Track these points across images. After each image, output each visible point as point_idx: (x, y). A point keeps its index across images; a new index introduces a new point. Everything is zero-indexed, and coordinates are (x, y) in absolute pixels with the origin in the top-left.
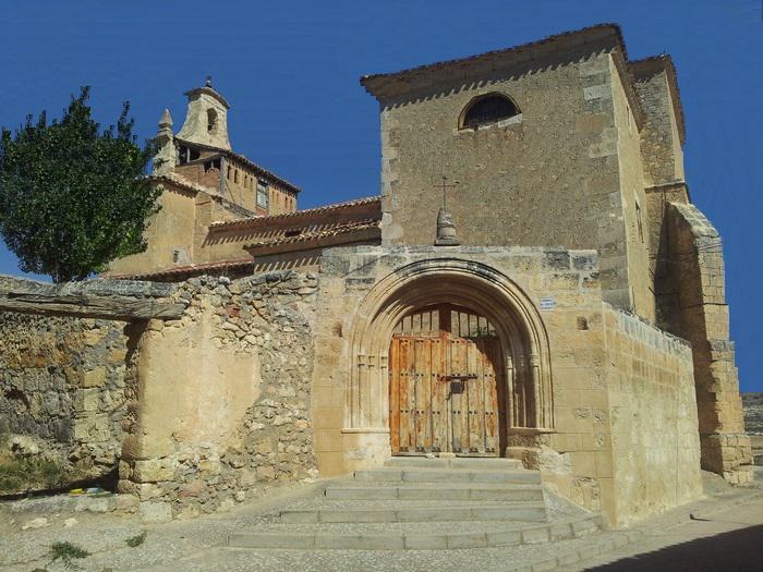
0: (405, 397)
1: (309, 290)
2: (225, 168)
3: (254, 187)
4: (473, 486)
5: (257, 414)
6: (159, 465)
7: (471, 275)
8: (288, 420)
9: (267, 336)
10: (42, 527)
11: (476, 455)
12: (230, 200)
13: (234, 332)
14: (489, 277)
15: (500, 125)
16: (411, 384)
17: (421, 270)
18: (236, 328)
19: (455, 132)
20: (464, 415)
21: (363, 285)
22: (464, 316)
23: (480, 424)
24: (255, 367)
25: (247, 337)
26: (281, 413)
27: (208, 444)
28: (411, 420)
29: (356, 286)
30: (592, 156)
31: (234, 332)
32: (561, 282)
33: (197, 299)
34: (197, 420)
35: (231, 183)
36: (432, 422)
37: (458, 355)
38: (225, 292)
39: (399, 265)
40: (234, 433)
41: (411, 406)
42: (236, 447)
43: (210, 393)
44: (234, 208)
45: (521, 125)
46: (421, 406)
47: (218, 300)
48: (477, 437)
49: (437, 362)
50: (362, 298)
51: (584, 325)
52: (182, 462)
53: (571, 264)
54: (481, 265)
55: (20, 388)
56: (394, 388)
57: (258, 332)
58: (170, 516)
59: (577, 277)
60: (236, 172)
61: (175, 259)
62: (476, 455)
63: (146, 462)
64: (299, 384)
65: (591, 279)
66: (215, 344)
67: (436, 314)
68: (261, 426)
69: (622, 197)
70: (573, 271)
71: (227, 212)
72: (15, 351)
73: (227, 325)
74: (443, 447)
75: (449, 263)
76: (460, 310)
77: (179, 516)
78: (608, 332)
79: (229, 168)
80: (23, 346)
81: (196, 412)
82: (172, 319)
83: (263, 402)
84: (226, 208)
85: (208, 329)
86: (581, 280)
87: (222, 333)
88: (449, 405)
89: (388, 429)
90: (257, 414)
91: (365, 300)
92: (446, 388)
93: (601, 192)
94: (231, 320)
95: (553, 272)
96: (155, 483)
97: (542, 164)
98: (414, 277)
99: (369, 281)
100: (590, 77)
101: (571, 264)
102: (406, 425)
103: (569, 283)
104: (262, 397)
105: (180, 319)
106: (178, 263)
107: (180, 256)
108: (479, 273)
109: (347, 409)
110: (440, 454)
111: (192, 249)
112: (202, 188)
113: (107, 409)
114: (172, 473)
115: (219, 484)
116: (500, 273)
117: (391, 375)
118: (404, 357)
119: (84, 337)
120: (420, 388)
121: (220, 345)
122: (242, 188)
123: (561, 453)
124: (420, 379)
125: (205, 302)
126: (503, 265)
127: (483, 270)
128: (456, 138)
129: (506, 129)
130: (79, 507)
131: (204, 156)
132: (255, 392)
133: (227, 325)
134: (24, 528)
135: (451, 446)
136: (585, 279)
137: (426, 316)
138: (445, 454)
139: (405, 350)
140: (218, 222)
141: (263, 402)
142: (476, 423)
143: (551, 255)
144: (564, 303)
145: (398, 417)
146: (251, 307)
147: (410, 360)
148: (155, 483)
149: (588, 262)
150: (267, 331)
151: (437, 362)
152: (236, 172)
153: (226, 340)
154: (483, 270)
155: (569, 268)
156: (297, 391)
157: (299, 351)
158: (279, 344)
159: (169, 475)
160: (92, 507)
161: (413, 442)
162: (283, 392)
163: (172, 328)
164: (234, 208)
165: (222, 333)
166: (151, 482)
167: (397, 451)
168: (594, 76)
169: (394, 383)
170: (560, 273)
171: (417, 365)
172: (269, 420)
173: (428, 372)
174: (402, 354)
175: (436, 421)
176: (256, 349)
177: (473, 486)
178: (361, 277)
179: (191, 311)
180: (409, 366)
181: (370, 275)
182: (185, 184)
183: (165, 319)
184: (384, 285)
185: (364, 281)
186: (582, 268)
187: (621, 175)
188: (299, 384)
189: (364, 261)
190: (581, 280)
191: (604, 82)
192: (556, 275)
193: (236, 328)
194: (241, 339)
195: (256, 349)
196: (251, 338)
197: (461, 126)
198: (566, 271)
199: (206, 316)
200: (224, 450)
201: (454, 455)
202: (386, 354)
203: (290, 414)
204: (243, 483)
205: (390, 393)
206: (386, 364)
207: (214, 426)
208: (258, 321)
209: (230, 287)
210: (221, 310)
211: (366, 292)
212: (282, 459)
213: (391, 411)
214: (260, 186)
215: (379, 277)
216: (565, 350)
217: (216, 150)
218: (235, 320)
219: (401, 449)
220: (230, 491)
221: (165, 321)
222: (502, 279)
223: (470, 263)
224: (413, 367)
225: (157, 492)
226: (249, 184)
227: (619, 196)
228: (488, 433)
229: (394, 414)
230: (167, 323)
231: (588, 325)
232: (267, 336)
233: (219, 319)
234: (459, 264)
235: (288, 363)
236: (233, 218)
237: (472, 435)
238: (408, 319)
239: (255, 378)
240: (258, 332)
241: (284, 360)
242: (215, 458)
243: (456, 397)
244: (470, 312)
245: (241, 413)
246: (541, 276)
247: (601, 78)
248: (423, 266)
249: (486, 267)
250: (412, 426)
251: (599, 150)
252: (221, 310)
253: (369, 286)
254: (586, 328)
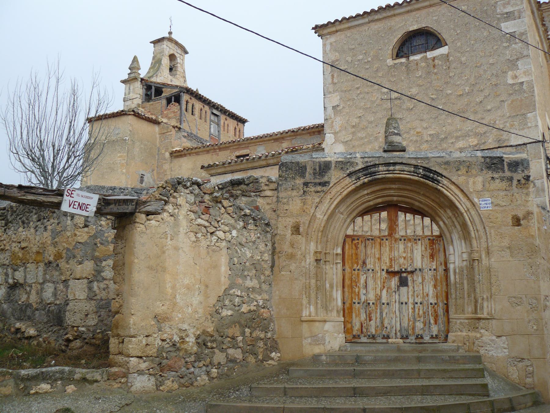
0: (357, 290)
1: (268, 193)
2: (184, 103)
3: (208, 119)
4: (422, 366)
5: (227, 302)
6: (144, 342)
7: (416, 178)
8: (253, 308)
9: (234, 233)
10: (46, 392)
11: (421, 341)
12: (187, 129)
13: (205, 227)
14: (433, 180)
15: (430, 54)
16: (362, 279)
17: (372, 174)
18: (207, 224)
19: (390, 62)
20: (411, 306)
21: (319, 188)
22: (409, 216)
23: (424, 313)
24: (224, 260)
25: (217, 233)
26: (247, 303)
27: (185, 326)
28: (362, 311)
29: (313, 189)
30: (510, 81)
31: (205, 227)
32: (497, 184)
33: (174, 197)
34: (175, 304)
35: (188, 115)
36: (381, 313)
37: (405, 252)
38: (197, 191)
39: (352, 169)
40: (207, 318)
41: (363, 298)
42: (209, 330)
43: (186, 281)
44: (190, 136)
45: (448, 55)
46: (371, 297)
47: (191, 198)
48: (422, 326)
49: (386, 258)
50: (318, 200)
51: (517, 221)
52: (163, 340)
53: (506, 167)
54: (425, 169)
55: (21, 281)
56: (347, 282)
57: (227, 229)
58: (155, 387)
59: (511, 179)
60: (193, 106)
61: (142, 181)
62: (421, 341)
63: (133, 339)
64: (262, 277)
65: (523, 181)
66: (189, 238)
67: (384, 214)
68: (230, 313)
69: (538, 118)
70: (508, 174)
71: (185, 140)
72: (17, 249)
73: (199, 221)
74: (393, 334)
75: (397, 167)
76: (406, 210)
77: (161, 388)
78: (539, 228)
79: (187, 102)
80: (23, 245)
81: (175, 297)
82: (153, 214)
83: (231, 292)
84: (185, 137)
85: (184, 224)
86: (515, 182)
87: (195, 228)
88: (397, 297)
89: (342, 319)
90: (227, 302)
91: (320, 202)
92: (395, 281)
93: (519, 113)
94: (203, 217)
95: (490, 174)
96: (141, 357)
97: (467, 89)
98: (366, 180)
99: (324, 184)
100: (507, 13)
101: (506, 167)
102: (358, 315)
103: (504, 184)
104: (231, 287)
105: (159, 214)
106: (144, 185)
107: (145, 178)
108: (424, 177)
109: (305, 301)
110: (390, 340)
111: (155, 172)
112: (165, 120)
113: (95, 298)
114: (155, 350)
115: (195, 361)
116: (442, 176)
117: (344, 270)
118: (356, 254)
119: (76, 235)
120: (370, 283)
121: (194, 239)
122: (198, 119)
123: (499, 337)
124: (371, 274)
125: (181, 200)
126: (446, 169)
127: (428, 174)
128: (390, 67)
129: (434, 59)
130: (77, 376)
131: (167, 92)
132: (225, 282)
133: (199, 221)
134: (32, 392)
135: (398, 334)
136: (519, 181)
137: (376, 216)
138: (394, 340)
139: (357, 248)
140: (178, 149)
141: (231, 292)
142: (421, 312)
143: (488, 160)
144: (500, 203)
145: (351, 308)
146: (220, 206)
147: (362, 256)
148: (141, 357)
149: (520, 166)
150: (235, 228)
151: (386, 258)
152: (193, 106)
153: (199, 235)
154: (428, 174)
155: (504, 172)
156: (260, 283)
157: (262, 247)
158: (244, 240)
159: (152, 351)
160: (89, 377)
161: (364, 330)
162: (249, 283)
163: (153, 222)
164: (190, 136)
165: (195, 228)
166: (138, 357)
167: (350, 337)
168: (510, 12)
169: (346, 277)
170: (496, 176)
171: (368, 261)
172: (237, 308)
173: (377, 268)
174: (354, 252)
175: (385, 311)
176: (224, 244)
177: (422, 366)
178: (317, 181)
179: (170, 208)
180: (360, 262)
181: (326, 179)
182: (150, 116)
183: (148, 214)
184: (338, 188)
185: (320, 184)
186: (516, 171)
187: (537, 98)
188: (262, 277)
189: (320, 166)
190: (515, 182)
191: (519, 18)
192: (493, 178)
193: (207, 224)
194: (212, 233)
195: (224, 244)
196: (220, 234)
197: (395, 57)
198: (501, 174)
199: (183, 211)
200: (198, 333)
201: (401, 341)
202: (339, 251)
203: (255, 303)
204: (215, 362)
205: (343, 287)
206: (340, 261)
207: (190, 310)
208: (227, 219)
209: (202, 187)
210: (195, 208)
211: (322, 194)
212: (249, 343)
213: (344, 303)
214: (213, 117)
215: (333, 181)
216: (503, 244)
217: (177, 86)
218: (206, 217)
219: (354, 337)
220: (204, 368)
221: (148, 215)
222: (445, 182)
223: (416, 167)
224: (364, 263)
225: (143, 366)
226: (203, 116)
227: (535, 117)
228: (432, 321)
229: (347, 305)
230: (150, 217)
231: (522, 222)
232: (234, 233)
233: (192, 216)
234: (406, 168)
235: (252, 257)
236: (188, 144)
237: (418, 324)
238: (359, 219)
239: (224, 269)
240: (227, 229)
241: (249, 255)
242: (191, 340)
243: (404, 289)
244: (415, 211)
245: (213, 300)
246: (480, 179)
247: (516, 14)
248: (373, 170)
249: (430, 171)
250: (363, 316)
251: (516, 77)
252: (195, 208)
253: (324, 188)
254: (519, 225)
